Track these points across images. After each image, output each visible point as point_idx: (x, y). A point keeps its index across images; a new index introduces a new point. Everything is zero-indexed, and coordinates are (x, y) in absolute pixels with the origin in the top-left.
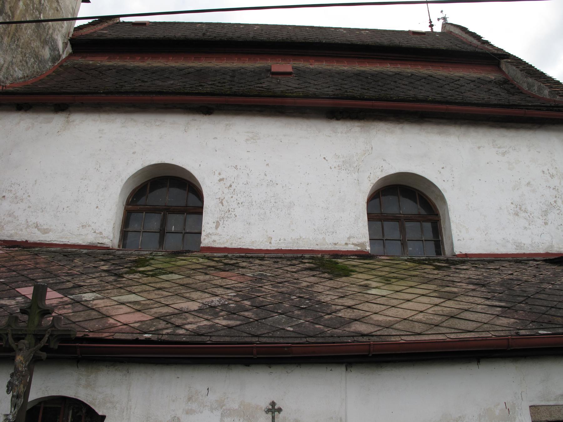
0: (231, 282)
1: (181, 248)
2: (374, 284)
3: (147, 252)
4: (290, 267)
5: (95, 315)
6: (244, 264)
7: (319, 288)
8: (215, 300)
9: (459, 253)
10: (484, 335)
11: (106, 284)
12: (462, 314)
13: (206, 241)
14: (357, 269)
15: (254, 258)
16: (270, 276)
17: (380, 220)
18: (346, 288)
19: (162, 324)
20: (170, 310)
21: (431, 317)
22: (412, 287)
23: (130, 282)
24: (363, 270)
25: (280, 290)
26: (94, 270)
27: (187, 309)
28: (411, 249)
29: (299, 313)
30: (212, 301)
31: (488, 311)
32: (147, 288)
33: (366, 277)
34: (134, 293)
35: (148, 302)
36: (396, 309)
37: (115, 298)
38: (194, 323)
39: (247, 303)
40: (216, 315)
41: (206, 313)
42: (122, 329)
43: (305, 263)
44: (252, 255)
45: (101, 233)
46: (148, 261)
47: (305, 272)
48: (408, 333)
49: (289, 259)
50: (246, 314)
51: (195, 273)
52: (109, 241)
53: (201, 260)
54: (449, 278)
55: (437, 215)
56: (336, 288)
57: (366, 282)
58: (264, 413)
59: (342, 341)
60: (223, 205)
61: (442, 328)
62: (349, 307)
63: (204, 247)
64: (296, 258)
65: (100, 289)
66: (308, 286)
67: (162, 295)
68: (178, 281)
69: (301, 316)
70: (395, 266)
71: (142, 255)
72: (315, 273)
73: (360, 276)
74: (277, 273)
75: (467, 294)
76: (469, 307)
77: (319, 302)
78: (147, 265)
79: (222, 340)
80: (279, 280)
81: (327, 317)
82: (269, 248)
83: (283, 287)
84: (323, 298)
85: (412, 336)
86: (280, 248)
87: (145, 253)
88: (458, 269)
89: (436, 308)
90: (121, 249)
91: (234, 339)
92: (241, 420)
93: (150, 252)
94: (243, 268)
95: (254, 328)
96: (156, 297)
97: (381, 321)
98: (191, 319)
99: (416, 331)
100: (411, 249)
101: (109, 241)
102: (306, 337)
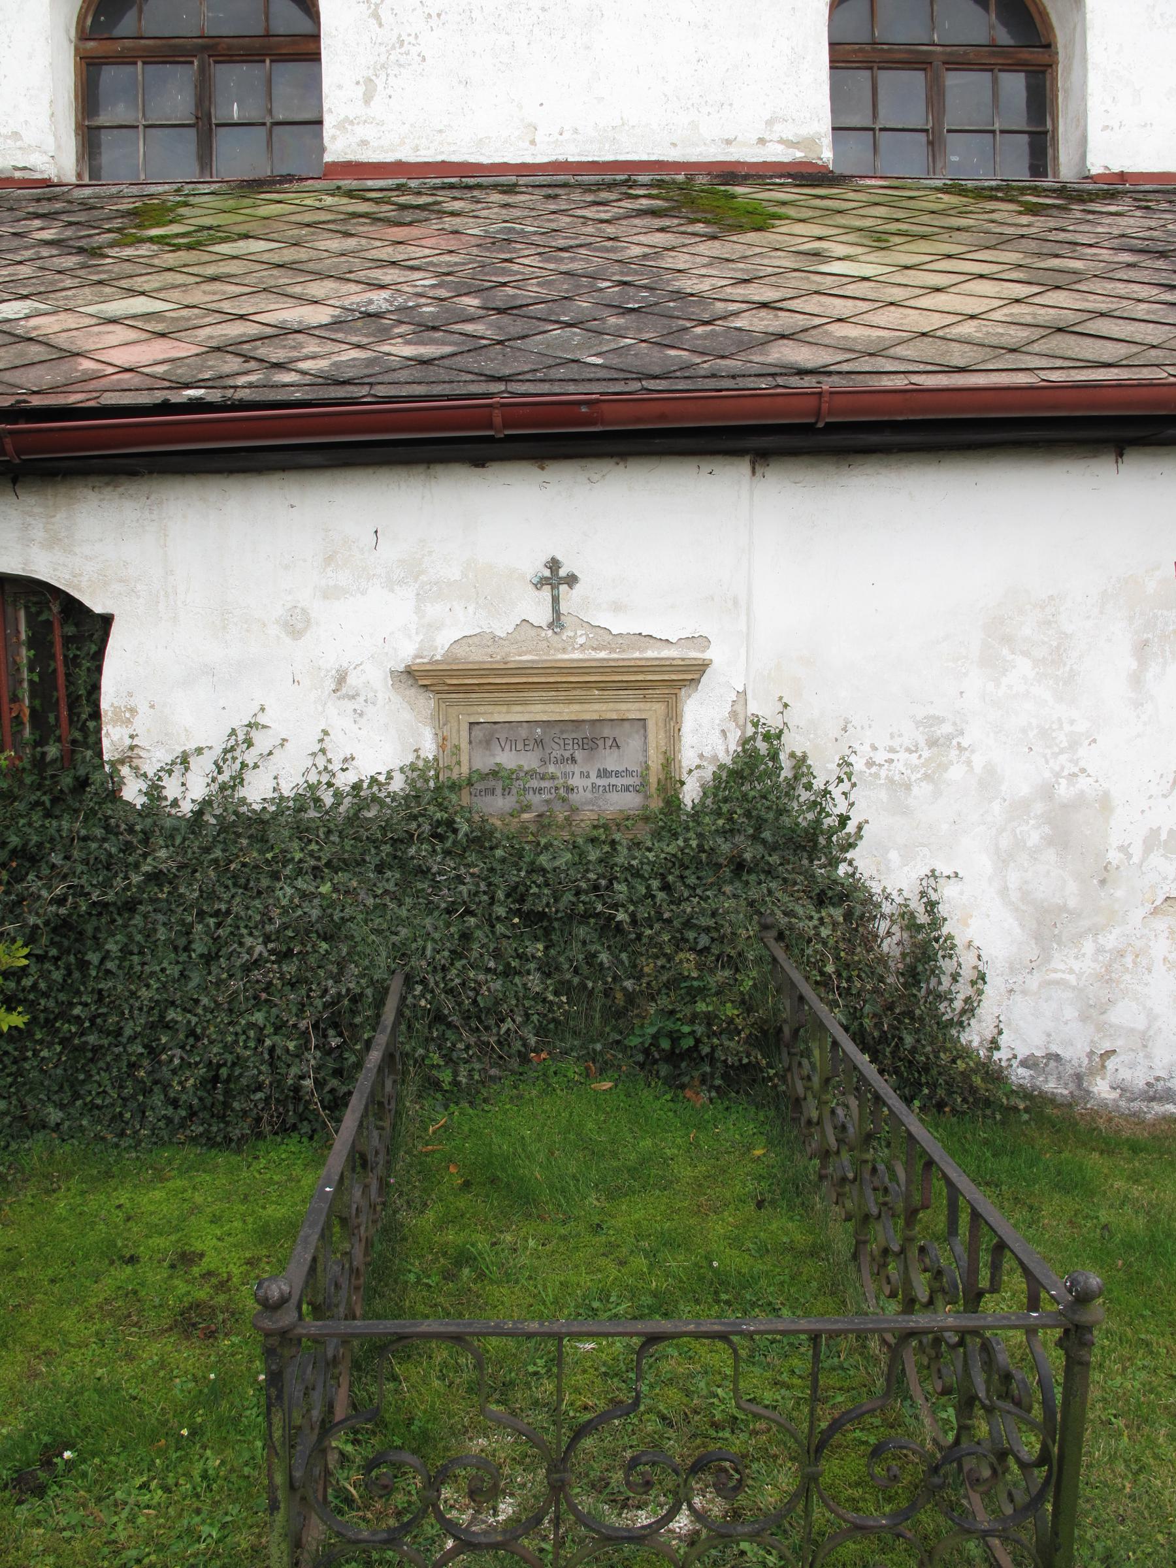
0: (420, 252)
1: (263, 171)
2: (840, 250)
3: (167, 187)
4: (595, 208)
5: (38, 353)
6: (457, 205)
7: (680, 261)
8: (379, 300)
9: (1101, 171)
10: (1146, 374)
11: (57, 277)
12: (1088, 324)
13: (340, 143)
14: (791, 212)
15: (487, 187)
16: (535, 233)
17: (868, 65)
18: (758, 260)
19: (232, 364)
20: (251, 329)
21: (1001, 330)
22: (949, 256)
23: (128, 268)
24: (810, 213)
25: (563, 268)
26: (16, 242)
27: (300, 322)
28: (955, 158)
29: (622, 321)
30: (371, 302)
31: (1165, 316)
32: (180, 279)
33: (818, 231)
34: (143, 293)
35: (185, 313)
36: (901, 310)
37: (90, 309)
38: (322, 357)
39: (472, 301)
40: (385, 335)
41: (356, 331)
42: (119, 380)
43: (638, 197)
44: (479, 180)
45: (16, 135)
46: (171, 210)
47: (637, 221)
48: (930, 368)
49: (587, 188)
50: (469, 328)
51: (313, 234)
52: (46, 159)
53: (329, 200)
54: (1062, 236)
55: (1049, 47)
56: (728, 260)
57: (817, 245)
58: (531, 587)
59: (741, 386)
60: (381, 25)
61: (1028, 357)
62: (764, 305)
63: (334, 164)
64: (610, 186)
65: (42, 289)
66: (645, 256)
67: (224, 293)
68: (265, 257)
69: (627, 328)
70: (905, 204)
71: (151, 196)
72: (666, 222)
73: (799, 228)
74: (554, 226)
75: (1110, 275)
76: (1114, 306)
77: (680, 295)
78: (171, 222)
79: (405, 391)
80: (561, 243)
81: (699, 330)
82: (529, 160)
83: (572, 259)
84: (687, 285)
85: (940, 376)
86: (561, 158)
87: (160, 189)
88: (1093, 212)
89: (1016, 309)
90: (86, 181)
91: (437, 390)
92: (471, 609)
93: (175, 187)
94: (453, 214)
95: (492, 360)
96: (208, 298)
97: (855, 339)
98: (312, 347)
99: (954, 363)
100: (955, 158)
101: (46, 159)
102: (640, 380)
